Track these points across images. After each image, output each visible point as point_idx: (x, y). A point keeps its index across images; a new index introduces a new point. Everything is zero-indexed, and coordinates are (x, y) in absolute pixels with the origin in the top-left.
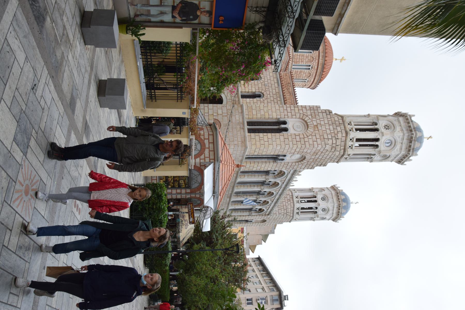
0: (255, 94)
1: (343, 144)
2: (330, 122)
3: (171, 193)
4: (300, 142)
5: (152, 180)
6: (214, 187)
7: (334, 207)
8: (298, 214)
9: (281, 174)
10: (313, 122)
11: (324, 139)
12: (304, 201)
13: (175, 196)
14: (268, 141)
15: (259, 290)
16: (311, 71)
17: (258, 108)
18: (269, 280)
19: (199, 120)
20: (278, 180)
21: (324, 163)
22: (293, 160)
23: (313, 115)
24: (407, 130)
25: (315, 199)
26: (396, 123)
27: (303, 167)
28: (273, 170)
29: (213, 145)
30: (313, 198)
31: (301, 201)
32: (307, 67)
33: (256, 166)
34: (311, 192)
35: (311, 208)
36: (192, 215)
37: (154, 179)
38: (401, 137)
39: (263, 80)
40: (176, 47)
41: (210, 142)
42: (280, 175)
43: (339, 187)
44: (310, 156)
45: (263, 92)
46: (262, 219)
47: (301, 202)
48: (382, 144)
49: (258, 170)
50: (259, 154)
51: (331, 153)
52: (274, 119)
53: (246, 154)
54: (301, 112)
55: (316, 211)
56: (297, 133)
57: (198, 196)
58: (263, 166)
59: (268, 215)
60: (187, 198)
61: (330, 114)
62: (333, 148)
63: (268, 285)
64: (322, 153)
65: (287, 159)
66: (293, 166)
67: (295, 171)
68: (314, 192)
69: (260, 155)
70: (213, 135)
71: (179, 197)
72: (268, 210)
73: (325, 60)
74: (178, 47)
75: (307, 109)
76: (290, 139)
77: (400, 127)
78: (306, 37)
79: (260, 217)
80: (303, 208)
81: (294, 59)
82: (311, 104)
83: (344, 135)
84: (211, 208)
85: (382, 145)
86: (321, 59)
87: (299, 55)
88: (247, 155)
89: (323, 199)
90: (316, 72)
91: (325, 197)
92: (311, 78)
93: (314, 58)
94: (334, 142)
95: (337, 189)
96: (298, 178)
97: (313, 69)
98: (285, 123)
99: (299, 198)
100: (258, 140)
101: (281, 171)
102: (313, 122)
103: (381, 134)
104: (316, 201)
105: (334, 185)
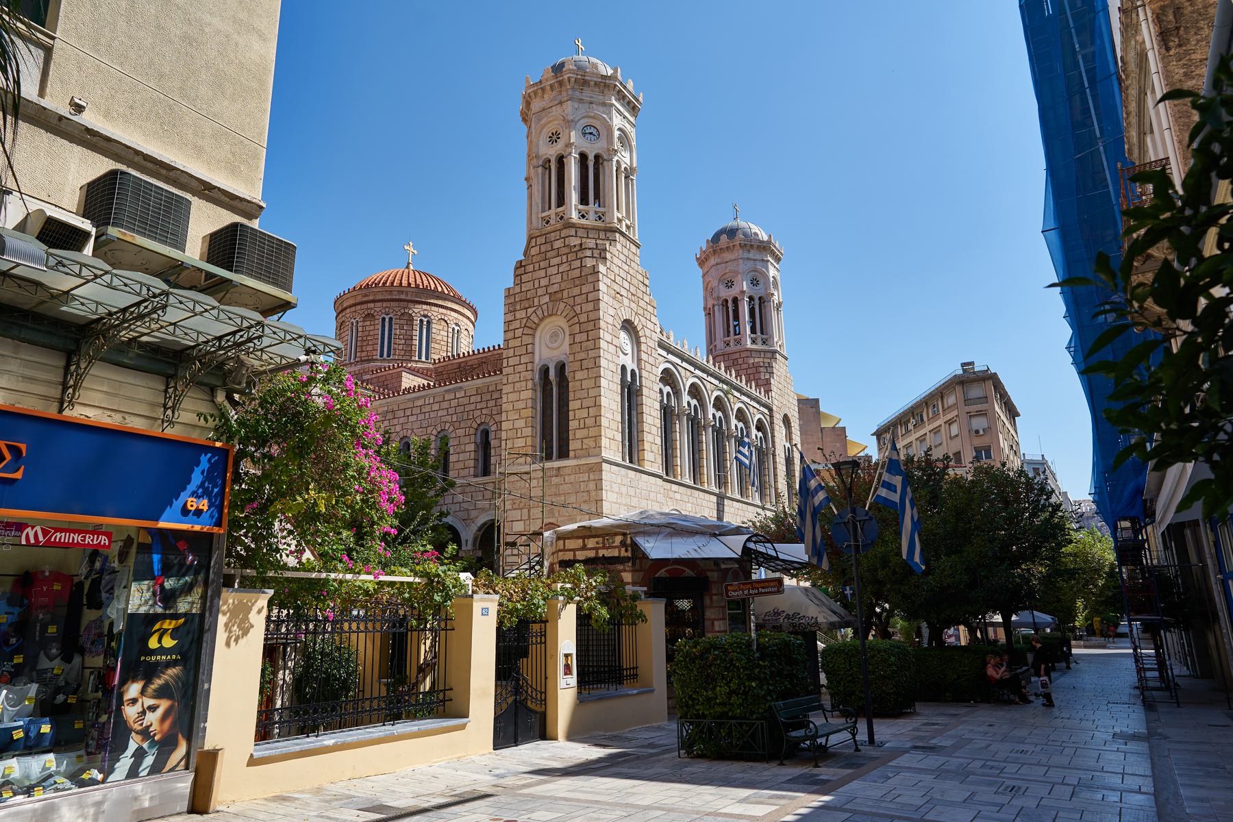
0: (481, 443)
2: (543, 264)
4: (590, 333)
7: (748, 259)
9: (668, 377)
10: (541, 303)
11: (581, 276)
15: (955, 429)
17: (510, 434)
25: (730, 304)
36: (757, 585)
38: (576, 105)
43: (701, 248)
44: (622, 309)
45: (475, 425)
47: (739, 334)
51: (615, 260)
54: (519, 333)
56: (567, 341)
59: (771, 410)
61: (525, 266)
62: (603, 255)
63: (941, 412)
64: (614, 281)
65: (631, 365)
66: (649, 349)
74: (350, 628)
76: (582, 356)
78: (250, 275)
79: (777, 428)
80: (753, 331)
82: (501, 309)
83: (572, 232)
97: (430, 315)
98: (545, 371)
101: (662, 380)
102: (541, 303)
104: (735, 301)
105: (697, 259)
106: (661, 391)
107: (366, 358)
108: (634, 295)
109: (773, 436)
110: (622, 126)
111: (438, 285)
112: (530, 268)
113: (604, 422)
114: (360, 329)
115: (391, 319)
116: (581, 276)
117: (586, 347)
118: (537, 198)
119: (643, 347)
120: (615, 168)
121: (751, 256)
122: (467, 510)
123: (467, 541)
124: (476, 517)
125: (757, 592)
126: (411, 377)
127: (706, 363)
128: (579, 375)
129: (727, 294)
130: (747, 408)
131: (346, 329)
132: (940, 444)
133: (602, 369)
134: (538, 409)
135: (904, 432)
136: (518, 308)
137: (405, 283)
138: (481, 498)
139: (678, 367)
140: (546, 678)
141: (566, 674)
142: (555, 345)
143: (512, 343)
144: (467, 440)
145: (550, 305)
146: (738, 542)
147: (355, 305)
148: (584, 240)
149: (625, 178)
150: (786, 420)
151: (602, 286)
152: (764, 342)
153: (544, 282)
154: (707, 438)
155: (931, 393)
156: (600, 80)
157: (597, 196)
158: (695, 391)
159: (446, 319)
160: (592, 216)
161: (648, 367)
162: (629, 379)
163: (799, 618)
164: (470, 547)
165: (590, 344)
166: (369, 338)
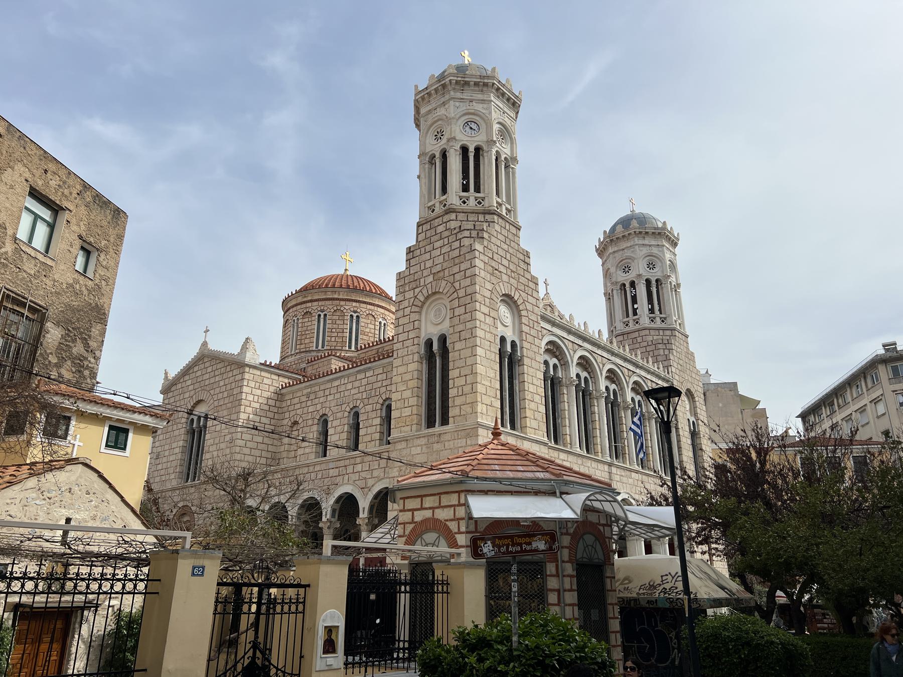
1: (472, 217)
2: (428, 248)
6: (537, 493)
8: (665, 318)
9: (554, 349)
10: (426, 283)
15: (881, 409)
16: (361, 313)
18: (851, 388)
20: (574, 358)
21: (522, 257)
23: (413, 285)
24: (444, 94)
25: (628, 285)
27: (531, 299)
29: (428, 498)
32: (354, 321)
33: (533, 406)
36: (519, 540)
38: (457, 104)
41: (419, 507)
43: (600, 239)
45: (381, 401)
48: (473, 139)
51: (493, 240)
54: (407, 311)
58: (532, 388)
60: (575, 573)
61: (413, 251)
62: (480, 235)
63: (864, 390)
64: (492, 259)
65: (510, 336)
73: (341, 286)
75: (402, 299)
76: (461, 327)
77: (438, 109)
80: (652, 311)
81: (337, 348)
83: (453, 216)
84: (587, 499)
86: (339, 295)
87: (329, 338)
89: (627, 269)
92: (378, 313)
93: (335, 308)
94: (467, 233)
97: (359, 310)
98: (429, 343)
99: (627, 319)
100: (462, 399)
102: (426, 283)
103: (451, 144)
105: (597, 250)
107: (304, 350)
108: (514, 272)
110: (501, 121)
111: (372, 287)
113: (480, 388)
114: (300, 325)
115: (325, 315)
116: (460, 256)
117: (464, 319)
119: (524, 320)
121: (646, 242)
122: (365, 478)
123: (364, 508)
124: (373, 486)
125: (519, 548)
128: (458, 346)
130: (592, 355)
131: (289, 326)
132: (868, 423)
134: (424, 380)
136: (407, 289)
137: (337, 284)
138: (377, 467)
139: (565, 340)
140: (301, 657)
142: (439, 320)
144: (373, 415)
145: (434, 284)
147: (296, 305)
151: (478, 262)
152: (663, 321)
153: (428, 264)
154: (600, 410)
155: (853, 375)
156: (479, 80)
159: (373, 314)
160: (472, 202)
161: (530, 339)
163: (677, 593)
165: (468, 316)
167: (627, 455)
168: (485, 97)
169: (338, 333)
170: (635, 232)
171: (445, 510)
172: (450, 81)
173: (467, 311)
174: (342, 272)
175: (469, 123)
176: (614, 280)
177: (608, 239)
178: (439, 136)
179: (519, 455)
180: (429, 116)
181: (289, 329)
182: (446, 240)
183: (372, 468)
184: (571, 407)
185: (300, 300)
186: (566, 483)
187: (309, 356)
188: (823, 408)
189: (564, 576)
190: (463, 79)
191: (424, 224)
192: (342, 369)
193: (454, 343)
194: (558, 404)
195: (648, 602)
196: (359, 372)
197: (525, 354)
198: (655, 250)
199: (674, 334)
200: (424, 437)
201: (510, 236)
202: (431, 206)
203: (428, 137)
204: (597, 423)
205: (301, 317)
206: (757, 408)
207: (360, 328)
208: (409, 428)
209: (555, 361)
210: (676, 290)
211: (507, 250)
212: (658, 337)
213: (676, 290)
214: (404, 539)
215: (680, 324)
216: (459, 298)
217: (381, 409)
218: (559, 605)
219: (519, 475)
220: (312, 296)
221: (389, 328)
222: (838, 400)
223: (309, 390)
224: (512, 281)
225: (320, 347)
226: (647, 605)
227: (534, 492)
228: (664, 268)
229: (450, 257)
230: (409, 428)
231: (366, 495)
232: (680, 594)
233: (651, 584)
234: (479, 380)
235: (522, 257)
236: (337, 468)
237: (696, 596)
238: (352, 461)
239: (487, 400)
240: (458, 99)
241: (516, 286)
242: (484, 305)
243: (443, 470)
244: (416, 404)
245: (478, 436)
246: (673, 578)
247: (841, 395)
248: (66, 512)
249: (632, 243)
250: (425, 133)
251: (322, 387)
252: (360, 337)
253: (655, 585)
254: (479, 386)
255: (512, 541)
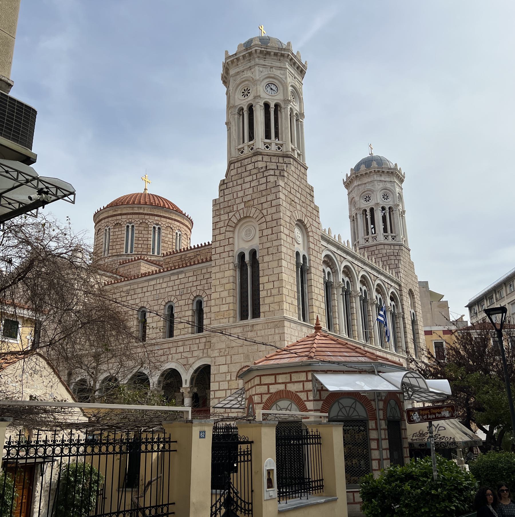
0: (197, 310)
1: (274, 159)
2: (239, 182)
3: (379, 460)
4: (274, 228)
5: (354, 503)
8: (395, 237)
9: (329, 261)
10: (239, 209)
11: (267, 189)
12: (373, 230)
13: (384, 452)
14: (273, 281)
16: (162, 225)
17: (218, 302)
18: (506, 287)
19: (237, 406)
21: (308, 191)
22: (304, 241)
23: (228, 210)
24: (250, 60)
26: (239, 79)
27: (315, 224)
28: (322, 273)
29: (280, 376)
30: (366, 215)
31: (372, 233)
32: (157, 232)
34: (357, 219)
35: (384, 218)
36: (434, 411)
37: (352, 497)
38: (261, 69)
39: (173, 298)
40: (100, 454)
41: (274, 382)
42: (330, 264)
43: (347, 175)
46: (408, 296)
47: (375, 233)
48: (273, 98)
49: (324, 299)
50: (296, 297)
51: (291, 178)
52: (236, 274)
53: (296, 319)
54: (223, 230)
55: (387, 209)
56: (258, 235)
57: (381, 405)
59: (400, 286)
60: (386, 427)
61: (226, 183)
62: (282, 174)
64: (290, 192)
67: (324, 238)
68: (356, 214)
69: (298, 296)
70: (260, 376)
71: (385, 444)
72: (391, 286)
73: (146, 204)
74: (146, 448)
75: (218, 220)
76: (269, 245)
79: (405, 298)
80: (385, 230)
81: (143, 253)
83: (260, 158)
84: (405, 376)
85: (275, 98)
86: (144, 210)
88: (299, 319)
89: (367, 199)
90: (165, 217)
91: (364, 196)
92: (175, 226)
93: (141, 221)
94: (272, 172)
95: (349, 177)
96: (334, 235)
98: (242, 256)
99: (367, 237)
100: (271, 299)
101: (324, 262)
102: (239, 209)
103: (257, 101)
104: (372, 210)
105: (344, 183)
106: (324, 271)
107: (116, 254)
108: (304, 203)
109: (402, 305)
111: (166, 204)
112: (231, 184)
113: (285, 291)
114: (111, 234)
115: (133, 226)
116: (267, 189)
117: (271, 238)
118: (234, 135)
119: (311, 239)
120: (289, 113)
122: (187, 358)
123: (186, 381)
124: (193, 363)
126: (147, 266)
127: (354, 252)
128: (266, 259)
129: (366, 205)
131: (101, 234)
133: (283, 254)
135: (489, 305)
136: (222, 212)
138: (196, 349)
139: (335, 254)
140: (252, 491)
141: (268, 487)
142: (249, 238)
143: (218, 238)
144: (186, 308)
145: (245, 210)
146: (398, 377)
147: (108, 217)
148: (268, 163)
149: (296, 120)
150: (411, 293)
152: (393, 239)
153: (240, 194)
154: (357, 304)
156: (277, 51)
157: (277, 136)
158: (347, 271)
159: (171, 226)
160: (274, 147)
161: (315, 253)
162: (302, 262)
163: (440, 438)
164: (188, 385)
165: (274, 237)
166: (118, 240)
167: (373, 338)
168: (282, 65)
169: (143, 241)
170: (375, 171)
171: (296, 384)
172: (256, 50)
173: (273, 233)
174: (142, 191)
175: (270, 85)
176: (357, 206)
177: (354, 175)
178: (246, 93)
179: (339, 344)
180: (238, 76)
181: (102, 237)
182: (255, 176)
183: (193, 350)
184: (339, 304)
185: (111, 213)
186: (382, 365)
187: (121, 259)
188: (485, 301)
189: (381, 429)
190: (265, 50)
191: (236, 162)
192: (154, 272)
193: (263, 256)
194: (330, 302)
195: (420, 445)
196: (173, 274)
197: (312, 265)
198: (388, 185)
199: (401, 249)
200: (240, 327)
201: (301, 175)
202: (240, 148)
203: (236, 94)
204: (355, 315)
205: (113, 227)
206: (441, 300)
207: (161, 238)
208: (227, 320)
209: (328, 269)
210: (402, 216)
211: (299, 185)
212: (390, 251)
213: (402, 216)
214: (262, 405)
215: (404, 241)
216: (266, 222)
217: (192, 304)
218: (378, 450)
219: (348, 359)
220: (122, 210)
221: (183, 238)
222: (496, 295)
223: (129, 287)
224: (303, 209)
225: (129, 252)
226: (419, 447)
227: (359, 371)
228: (395, 199)
229: (259, 190)
230: (227, 320)
231: (187, 370)
232: (443, 439)
233: (421, 432)
234: (284, 285)
235: (308, 191)
236: (162, 349)
237: (454, 440)
238: (175, 344)
239: (289, 300)
240: (262, 65)
241: (305, 213)
242: (286, 228)
243: (296, 356)
244: (232, 301)
245: (284, 326)
246: (436, 428)
247: (498, 292)
248: (30, 391)
249: (372, 179)
250: (234, 90)
251: (140, 286)
252: (161, 244)
253: (424, 433)
254: (284, 289)
255: (430, 412)
